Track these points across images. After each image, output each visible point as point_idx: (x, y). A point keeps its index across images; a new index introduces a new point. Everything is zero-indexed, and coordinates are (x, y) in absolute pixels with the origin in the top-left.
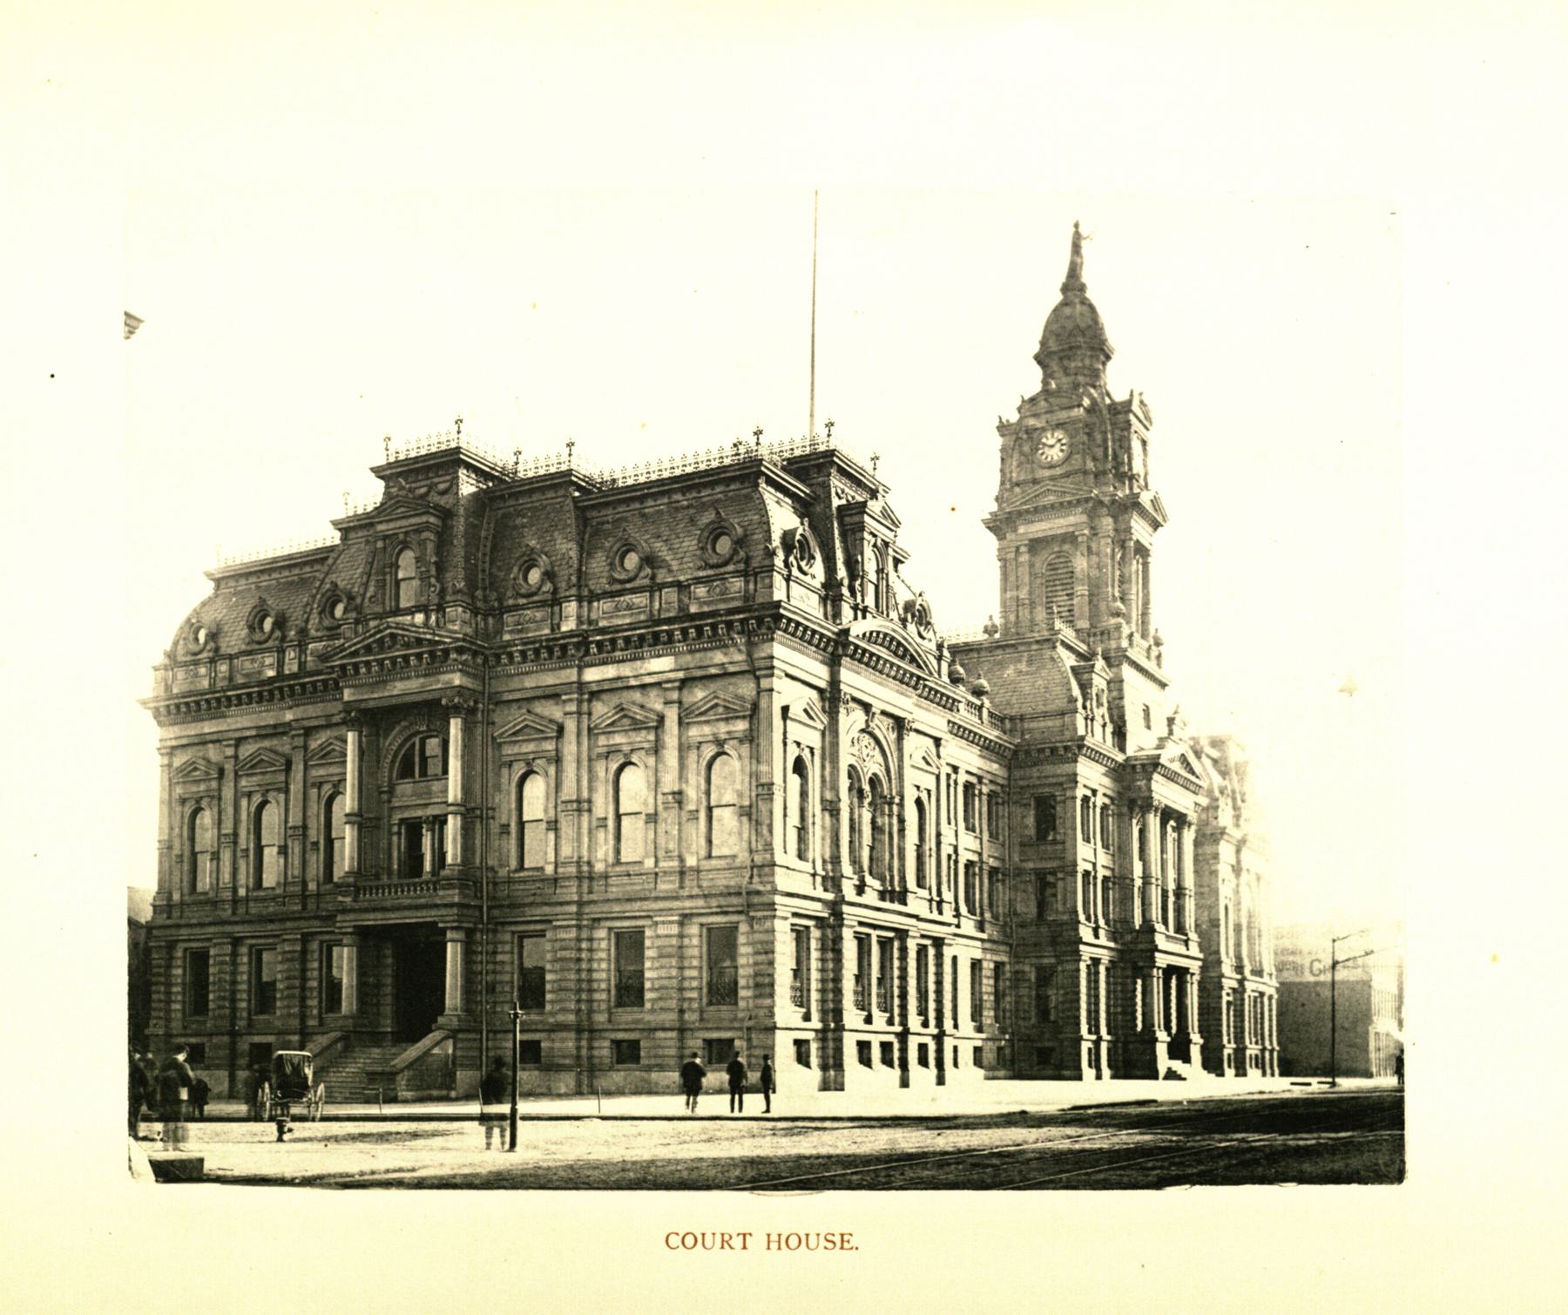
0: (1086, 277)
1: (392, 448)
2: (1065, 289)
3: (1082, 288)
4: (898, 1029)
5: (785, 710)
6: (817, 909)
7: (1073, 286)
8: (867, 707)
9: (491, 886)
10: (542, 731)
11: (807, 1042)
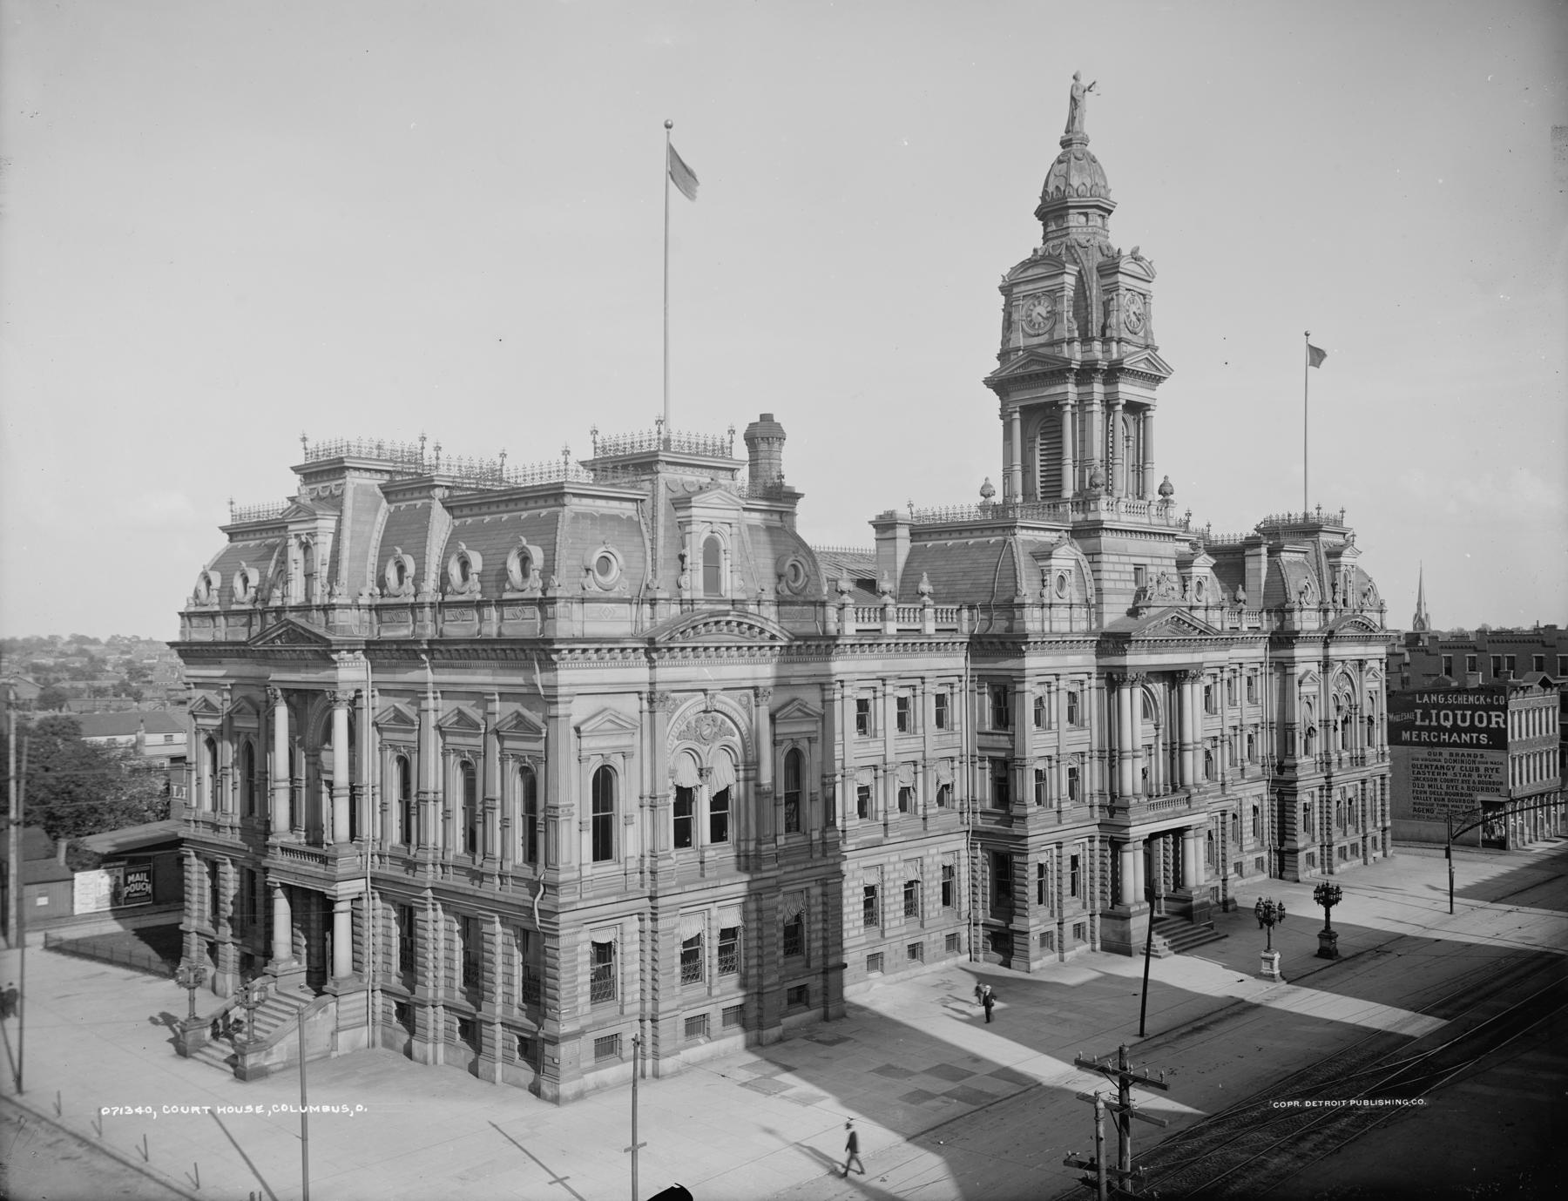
0: (1090, 125)
1: (311, 445)
2: (1066, 144)
8: (704, 691)
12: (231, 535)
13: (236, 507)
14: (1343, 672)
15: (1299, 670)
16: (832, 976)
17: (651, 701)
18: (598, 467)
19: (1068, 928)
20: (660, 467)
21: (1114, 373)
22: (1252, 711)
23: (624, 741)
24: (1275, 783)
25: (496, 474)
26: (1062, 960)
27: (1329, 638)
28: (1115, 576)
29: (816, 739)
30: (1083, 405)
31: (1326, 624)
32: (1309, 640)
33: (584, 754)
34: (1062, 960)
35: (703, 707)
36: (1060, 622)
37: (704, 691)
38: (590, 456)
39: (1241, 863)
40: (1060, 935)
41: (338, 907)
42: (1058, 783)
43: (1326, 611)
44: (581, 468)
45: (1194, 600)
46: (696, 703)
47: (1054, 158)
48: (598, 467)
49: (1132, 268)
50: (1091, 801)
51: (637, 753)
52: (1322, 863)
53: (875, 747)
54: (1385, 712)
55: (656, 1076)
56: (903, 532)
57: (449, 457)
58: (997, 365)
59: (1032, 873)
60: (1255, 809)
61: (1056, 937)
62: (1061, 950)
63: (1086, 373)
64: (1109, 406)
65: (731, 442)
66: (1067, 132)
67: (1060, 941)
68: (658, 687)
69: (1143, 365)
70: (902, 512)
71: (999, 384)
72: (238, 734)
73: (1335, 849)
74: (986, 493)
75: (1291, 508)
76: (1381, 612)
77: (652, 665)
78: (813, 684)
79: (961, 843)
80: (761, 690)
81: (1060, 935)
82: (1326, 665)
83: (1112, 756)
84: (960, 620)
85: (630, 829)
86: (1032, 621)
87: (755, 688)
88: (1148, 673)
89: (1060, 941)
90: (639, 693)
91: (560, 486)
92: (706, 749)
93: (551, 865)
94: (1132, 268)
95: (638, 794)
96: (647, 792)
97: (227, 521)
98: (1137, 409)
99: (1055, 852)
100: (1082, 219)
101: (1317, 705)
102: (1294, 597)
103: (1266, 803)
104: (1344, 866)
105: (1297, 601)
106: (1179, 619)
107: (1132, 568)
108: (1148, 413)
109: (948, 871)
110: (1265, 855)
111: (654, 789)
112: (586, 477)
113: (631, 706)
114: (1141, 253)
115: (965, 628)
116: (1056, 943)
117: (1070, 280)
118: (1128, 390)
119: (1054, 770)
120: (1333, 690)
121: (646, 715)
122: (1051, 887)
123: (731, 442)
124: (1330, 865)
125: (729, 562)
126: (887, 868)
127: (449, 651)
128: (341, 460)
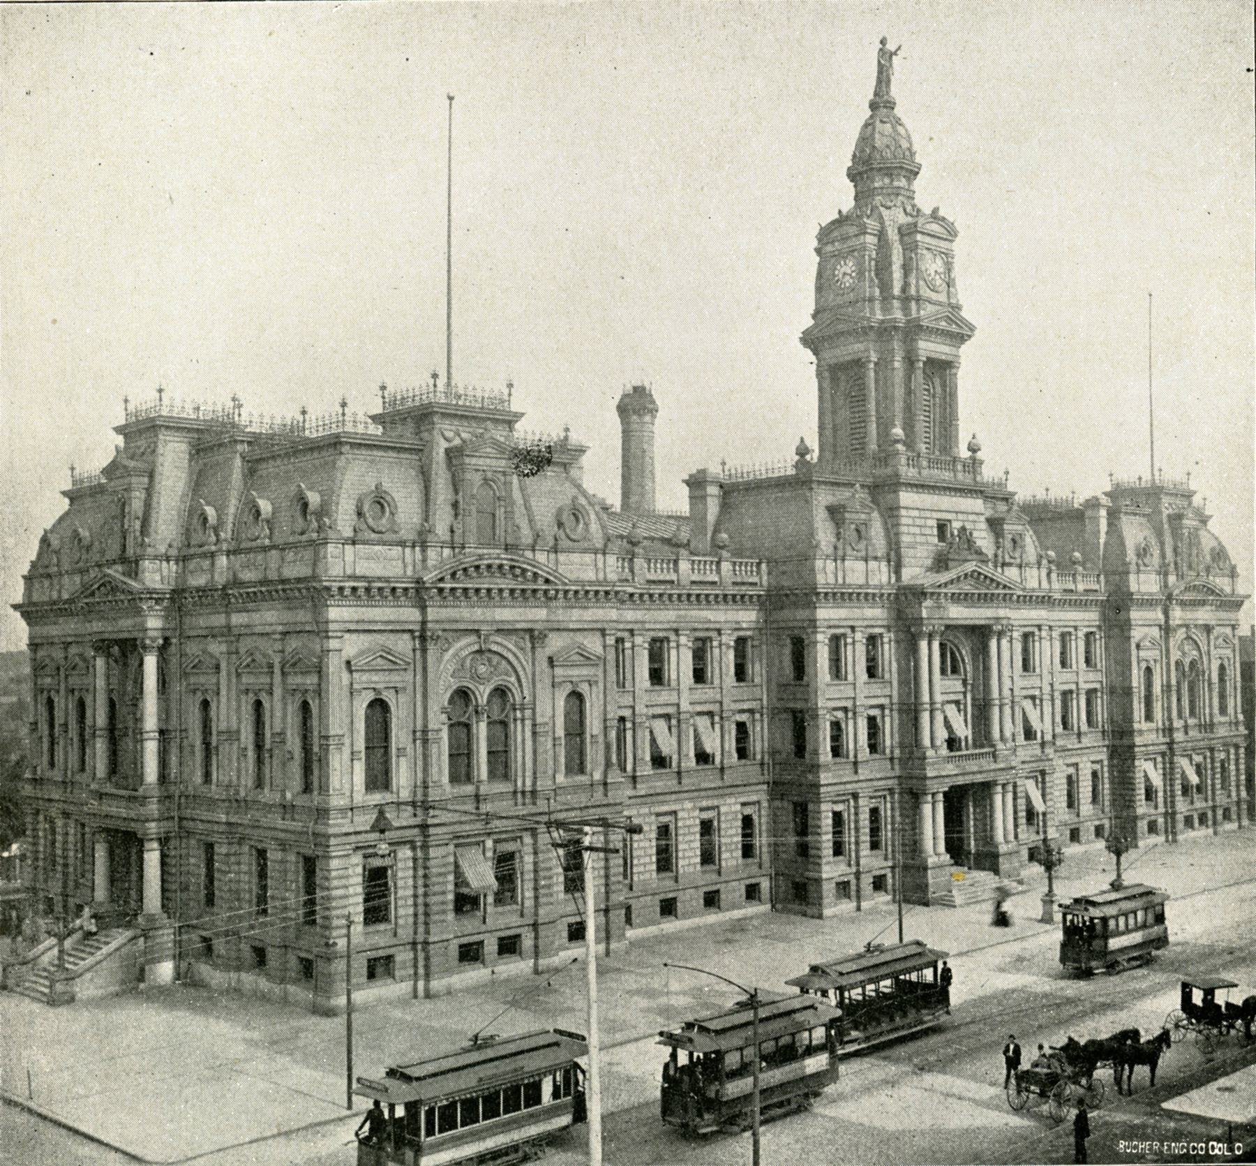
1: (131, 407)
2: (873, 106)
3: (891, 105)
4: (890, 863)
5: (1138, 646)
6: (1164, 748)
7: (881, 103)
9: (183, 800)
10: (395, 663)
11: (848, 882)
12: (72, 500)
13: (77, 472)
14: (1189, 638)
15: (1136, 634)
16: (603, 906)
17: (423, 638)
18: (388, 419)
19: (867, 881)
20: (436, 419)
21: (914, 330)
22: (1092, 676)
23: (395, 678)
24: (1113, 752)
25: (299, 428)
26: (859, 909)
27: (1167, 602)
28: (913, 530)
29: (596, 682)
30: (883, 364)
31: (1166, 586)
32: (1149, 603)
33: (356, 686)
34: (859, 909)
35: (476, 647)
36: (856, 572)
37: (477, 631)
38: (378, 410)
39: (1078, 829)
40: (858, 885)
41: (147, 845)
42: (857, 734)
43: (1166, 574)
44: (370, 421)
45: (1007, 557)
46: (465, 645)
47: (863, 122)
48: (388, 419)
49: (935, 228)
50: (892, 752)
51: (410, 688)
52: (1166, 832)
53: (665, 696)
54: (1239, 679)
55: (428, 995)
56: (713, 490)
57: (172, 399)
58: (812, 322)
59: (827, 822)
60: (1094, 774)
61: (853, 888)
62: (859, 898)
63: (884, 331)
64: (910, 361)
65: (510, 395)
66: (876, 94)
67: (858, 891)
68: (430, 625)
69: (944, 323)
70: (714, 469)
71: (810, 340)
72: (73, 691)
73: (1180, 817)
74: (802, 451)
75: (1135, 471)
76: (1232, 577)
77: (423, 608)
78: (592, 630)
79: (760, 794)
80: (536, 633)
81: (858, 885)
82: (1167, 629)
83: (910, 712)
84: (759, 573)
85: (403, 760)
86: (825, 573)
87: (531, 631)
88: (948, 627)
89: (858, 891)
90: (411, 631)
91: (337, 436)
92: (481, 688)
93: (324, 789)
94: (935, 228)
95: (411, 728)
96: (419, 726)
97: (68, 486)
98: (941, 369)
99: (852, 802)
100: (887, 181)
101: (1158, 670)
102: (1131, 556)
103: (1106, 769)
104: (1191, 834)
105: (1134, 562)
106: (980, 574)
107: (934, 523)
108: (954, 371)
109: (747, 822)
110: (1106, 823)
111: (425, 726)
112: (376, 430)
113: (404, 645)
114: (941, 213)
115: (765, 583)
116: (853, 893)
117: (871, 240)
118: (927, 347)
119: (851, 722)
120: (1175, 655)
121: (418, 653)
122: (849, 838)
123: (510, 395)
124: (1174, 834)
125: (503, 510)
126: (680, 815)
127: (241, 595)
128: (153, 419)
